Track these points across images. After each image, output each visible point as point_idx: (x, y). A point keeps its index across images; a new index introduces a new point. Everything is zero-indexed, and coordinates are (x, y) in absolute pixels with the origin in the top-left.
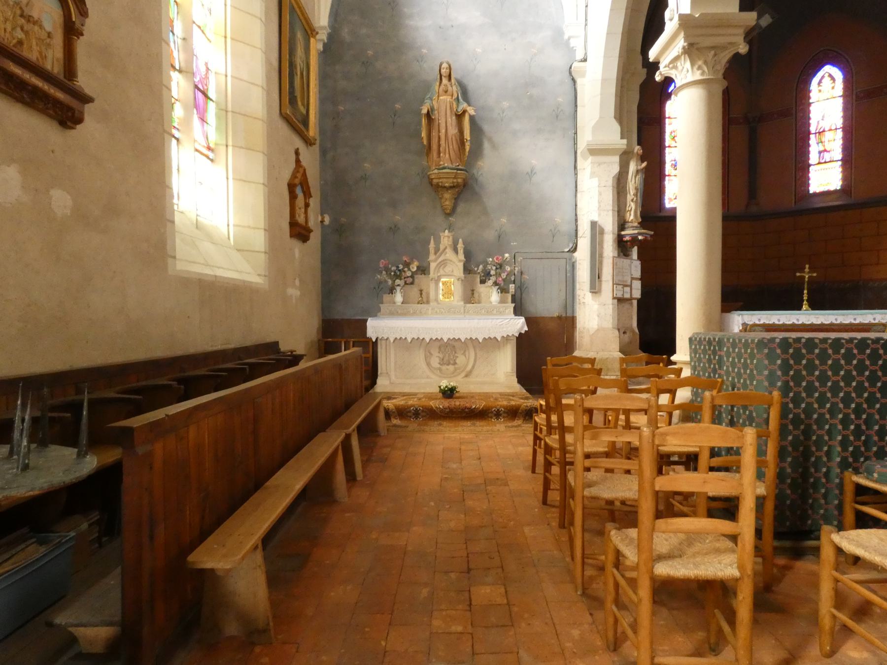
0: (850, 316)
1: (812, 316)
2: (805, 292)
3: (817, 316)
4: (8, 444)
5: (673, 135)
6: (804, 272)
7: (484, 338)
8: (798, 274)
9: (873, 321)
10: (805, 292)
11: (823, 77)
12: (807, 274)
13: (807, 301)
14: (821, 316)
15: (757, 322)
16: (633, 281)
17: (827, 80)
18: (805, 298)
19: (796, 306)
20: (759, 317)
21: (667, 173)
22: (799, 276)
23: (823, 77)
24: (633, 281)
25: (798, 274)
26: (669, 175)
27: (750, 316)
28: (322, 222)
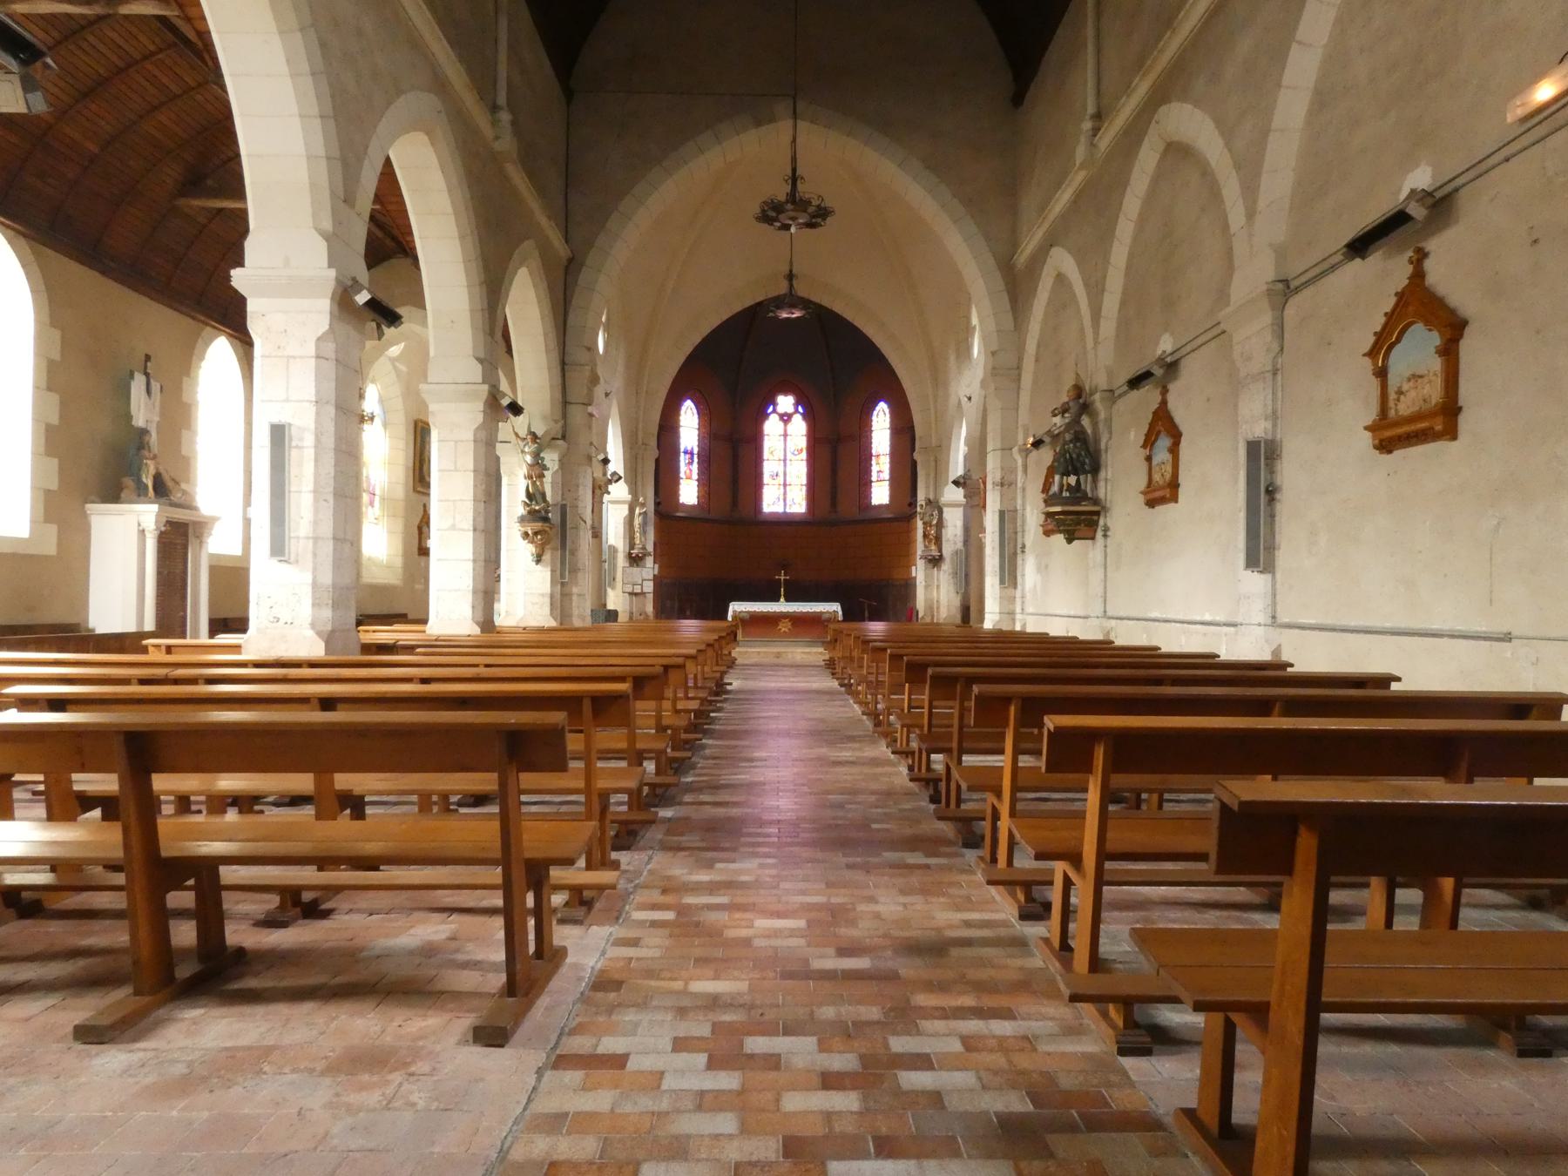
19: (776, 599)
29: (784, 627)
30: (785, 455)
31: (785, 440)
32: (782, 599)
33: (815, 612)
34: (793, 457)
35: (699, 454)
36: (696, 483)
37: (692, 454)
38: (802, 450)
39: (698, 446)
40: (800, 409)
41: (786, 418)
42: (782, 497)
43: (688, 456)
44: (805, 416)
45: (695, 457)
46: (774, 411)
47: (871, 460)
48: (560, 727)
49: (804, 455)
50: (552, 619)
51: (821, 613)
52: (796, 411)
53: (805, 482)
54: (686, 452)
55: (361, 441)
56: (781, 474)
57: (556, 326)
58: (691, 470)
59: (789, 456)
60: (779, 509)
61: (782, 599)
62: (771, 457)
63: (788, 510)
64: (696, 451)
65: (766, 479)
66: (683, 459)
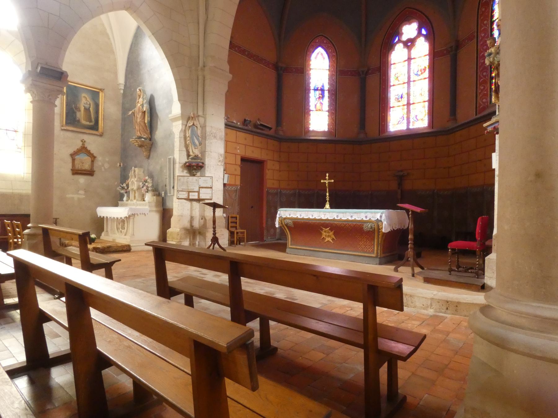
0: (348, 214)
1: (322, 213)
2: (327, 194)
3: (324, 213)
4: (192, 297)
5: (397, 76)
6: (326, 179)
7: (132, 214)
8: (322, 181)
9: (365, 219)
10: (327, 194)
11: (318, 54)
12: (327, 181)
13: (329, 202)
14: (327, 213)
15: (288, 216)
16: (200, 189)
17: (320, 55)
18: (328, 199)
19: (321, 206)
20: (289, 212)
21: (391, 105)
22: (323, 182)
23: (318, 54)
24: (200, 189)
25: (322, 181)
26: (393, 107)
27: (284, 212)
28: (120, 166)
29: (328, 236)
30: (409, 77)
31: (409, 65)
32: (327, 206)
33: (355, 221)
34: (416, 78)
35: (329, 90)
36: (327, 113)
37: (322, 90)
38: (425, 70)
39: (329, 84)
40: (424, 32)
41: (410, 44)
42: (405, 116)
43: (318, 93)
44: (427, 37)
45: (326, 94)
46: (399, 41)
47: (309, 93)
48: (146, 157)
49: (426, 74)
50: (260, 383)
51: (362, 222)
52: (420, 34)
53: (427, 98)
54: (316, 90)
55: (421, 128)
56: (405, 96)
57: (155, 110)
58: (321, 103)
59: (413, 77)
60: (403, 127)
61: (327, 206)
62: (396, 82)
63: (411, 127)
64: (326, 87)
65: (393, 102)
66: (313, 96)
